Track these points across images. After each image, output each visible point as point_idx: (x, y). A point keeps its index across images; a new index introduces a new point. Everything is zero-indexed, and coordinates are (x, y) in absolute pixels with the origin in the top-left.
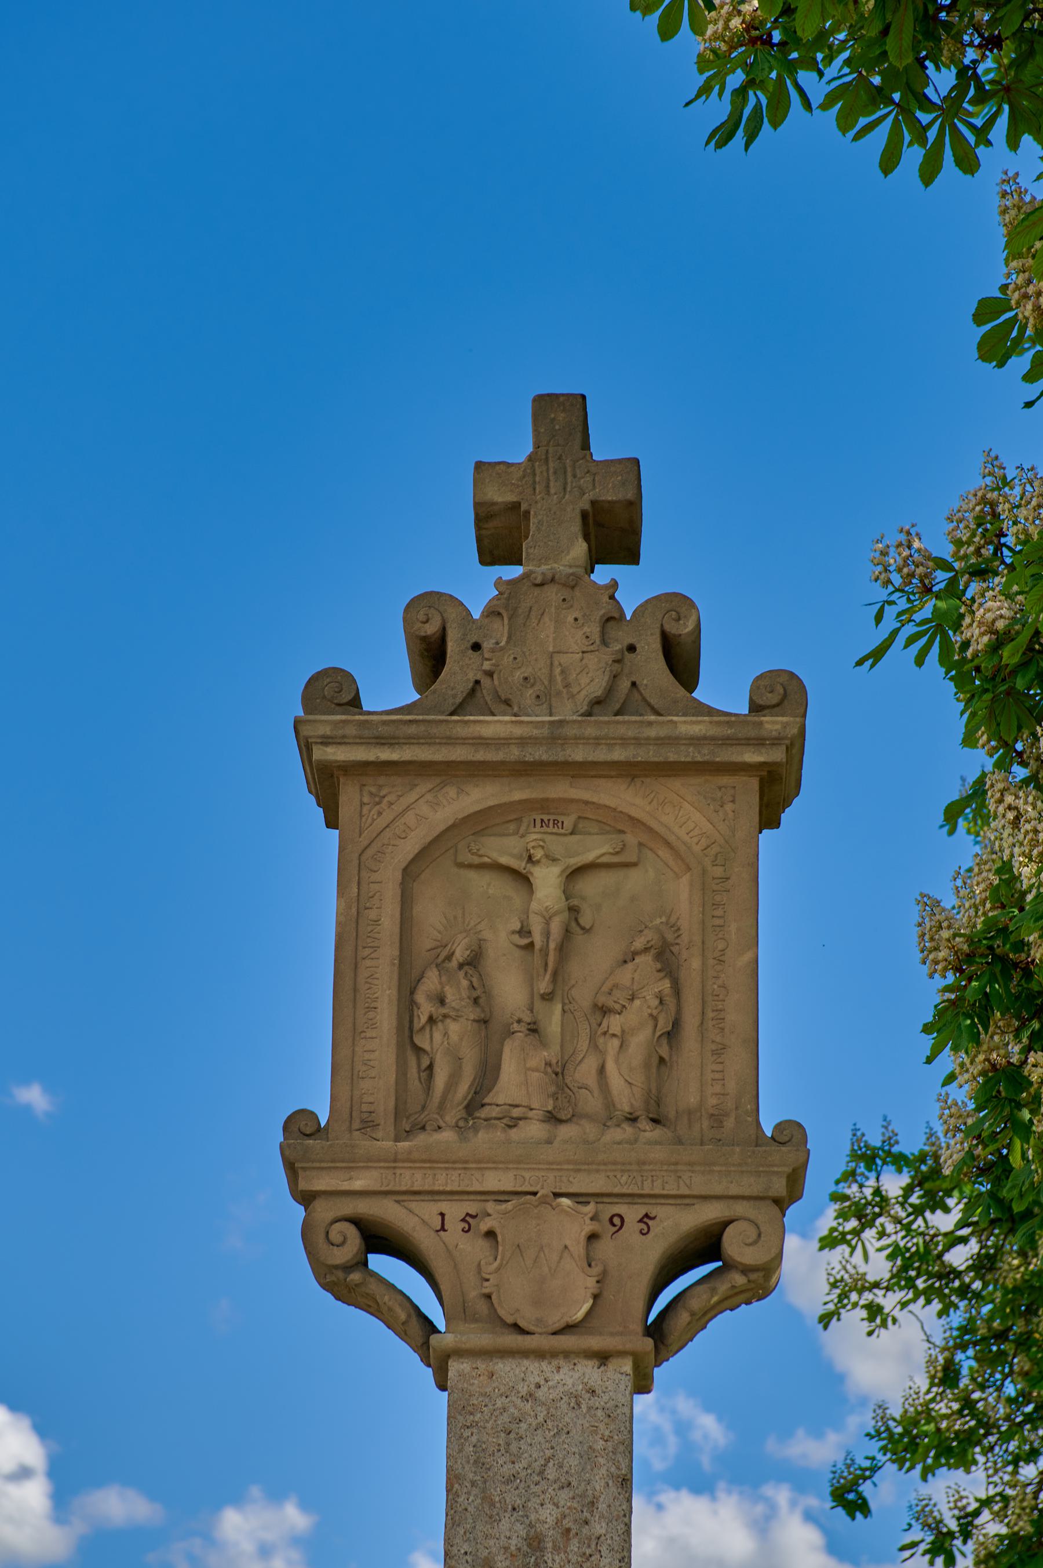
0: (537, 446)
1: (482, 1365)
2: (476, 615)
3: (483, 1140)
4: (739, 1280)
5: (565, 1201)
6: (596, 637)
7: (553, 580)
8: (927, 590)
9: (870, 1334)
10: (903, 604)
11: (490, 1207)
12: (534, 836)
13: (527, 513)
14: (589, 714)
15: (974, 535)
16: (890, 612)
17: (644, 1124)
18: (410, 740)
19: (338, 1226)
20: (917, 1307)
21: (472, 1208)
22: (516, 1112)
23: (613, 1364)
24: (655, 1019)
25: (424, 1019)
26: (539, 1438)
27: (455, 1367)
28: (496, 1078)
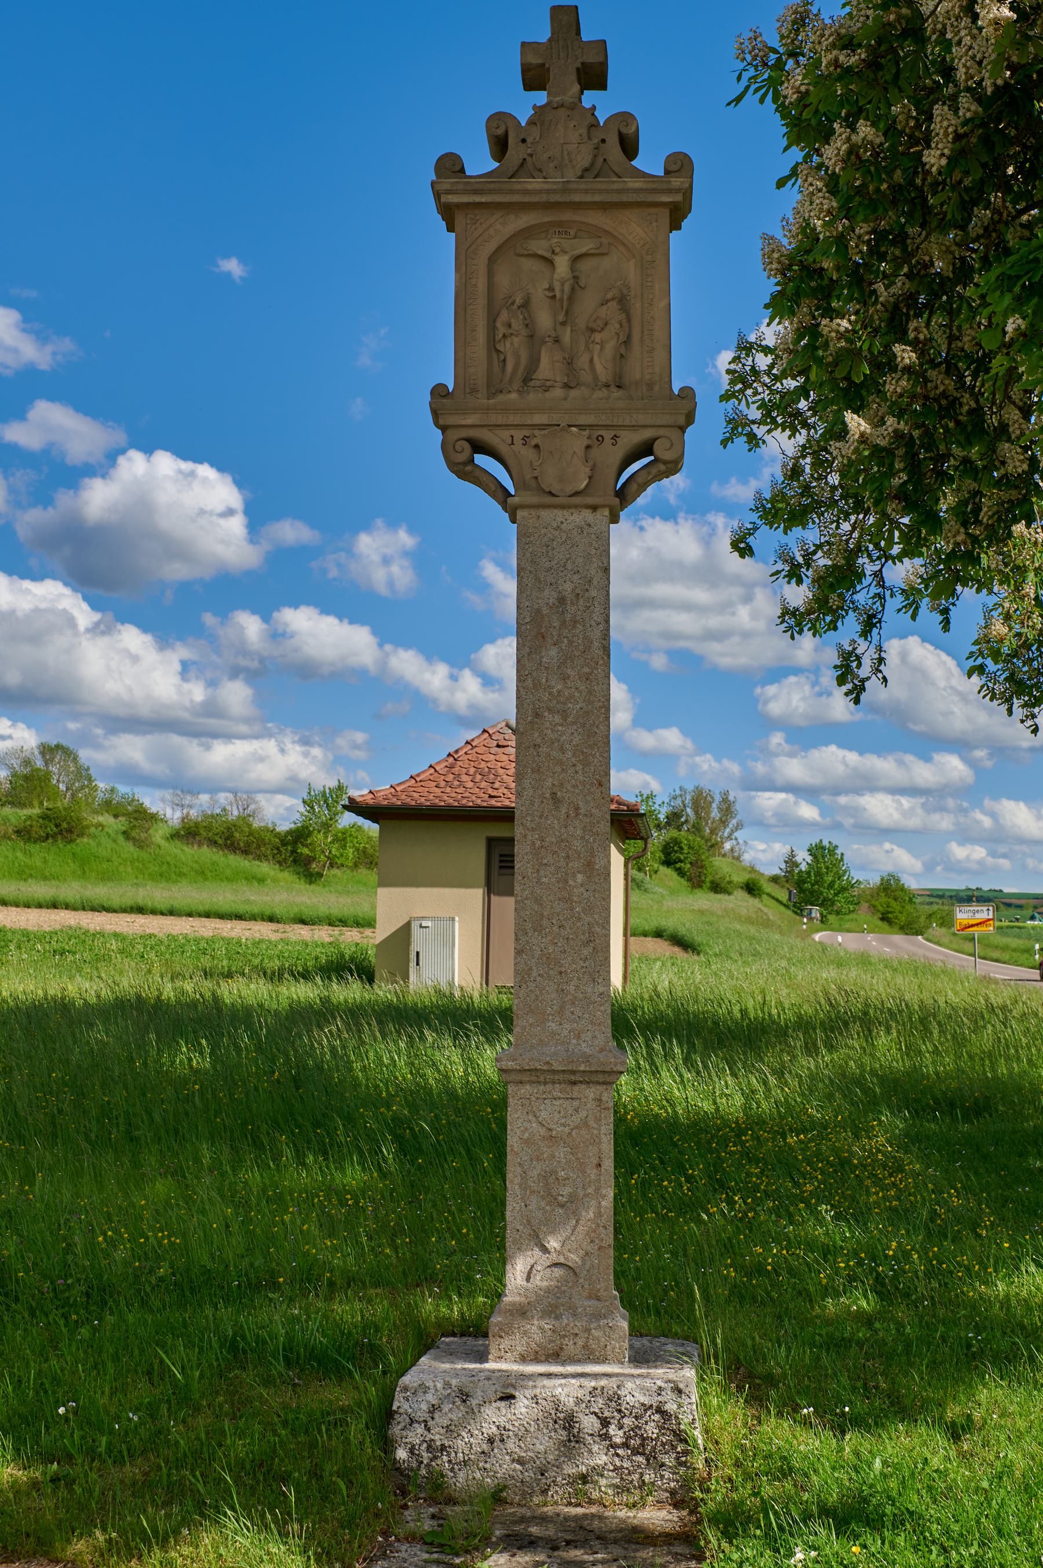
0: (553, 34)
1: (533, 512)
2: (523, 124)
3: (532, 397)
4: (662, 467)
5: (573, 429)
6: (585, 135)
7: (562, 105)
8: (765, 64)
9: (750, 450)
10: (752, 72)
11: (536, 432)
12: (555, 240)
13: (548, 69)
14: (581, 177)
15: (791, 32)
16: (746, 76)
17: (613, 389)
18: (490, 192)
19: (459, 442)
20: (777, 433)
21: (527, 433)
22: (548, 384)
23: (599, 512)
24: (618, 334)
25: (500, 336)
26: (563, 549)
27: (520, 514)
28: (537, 366)
